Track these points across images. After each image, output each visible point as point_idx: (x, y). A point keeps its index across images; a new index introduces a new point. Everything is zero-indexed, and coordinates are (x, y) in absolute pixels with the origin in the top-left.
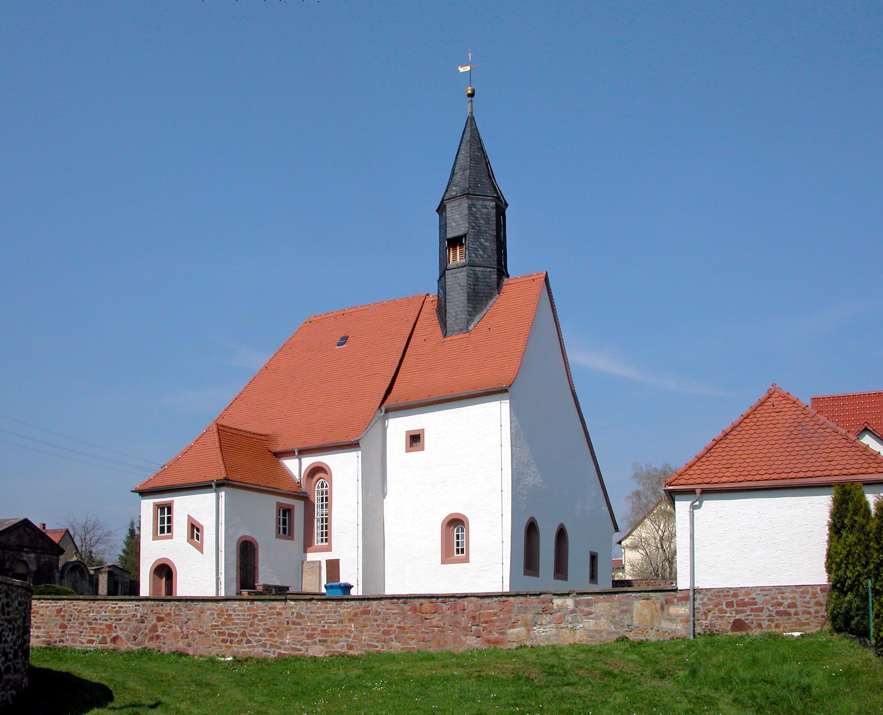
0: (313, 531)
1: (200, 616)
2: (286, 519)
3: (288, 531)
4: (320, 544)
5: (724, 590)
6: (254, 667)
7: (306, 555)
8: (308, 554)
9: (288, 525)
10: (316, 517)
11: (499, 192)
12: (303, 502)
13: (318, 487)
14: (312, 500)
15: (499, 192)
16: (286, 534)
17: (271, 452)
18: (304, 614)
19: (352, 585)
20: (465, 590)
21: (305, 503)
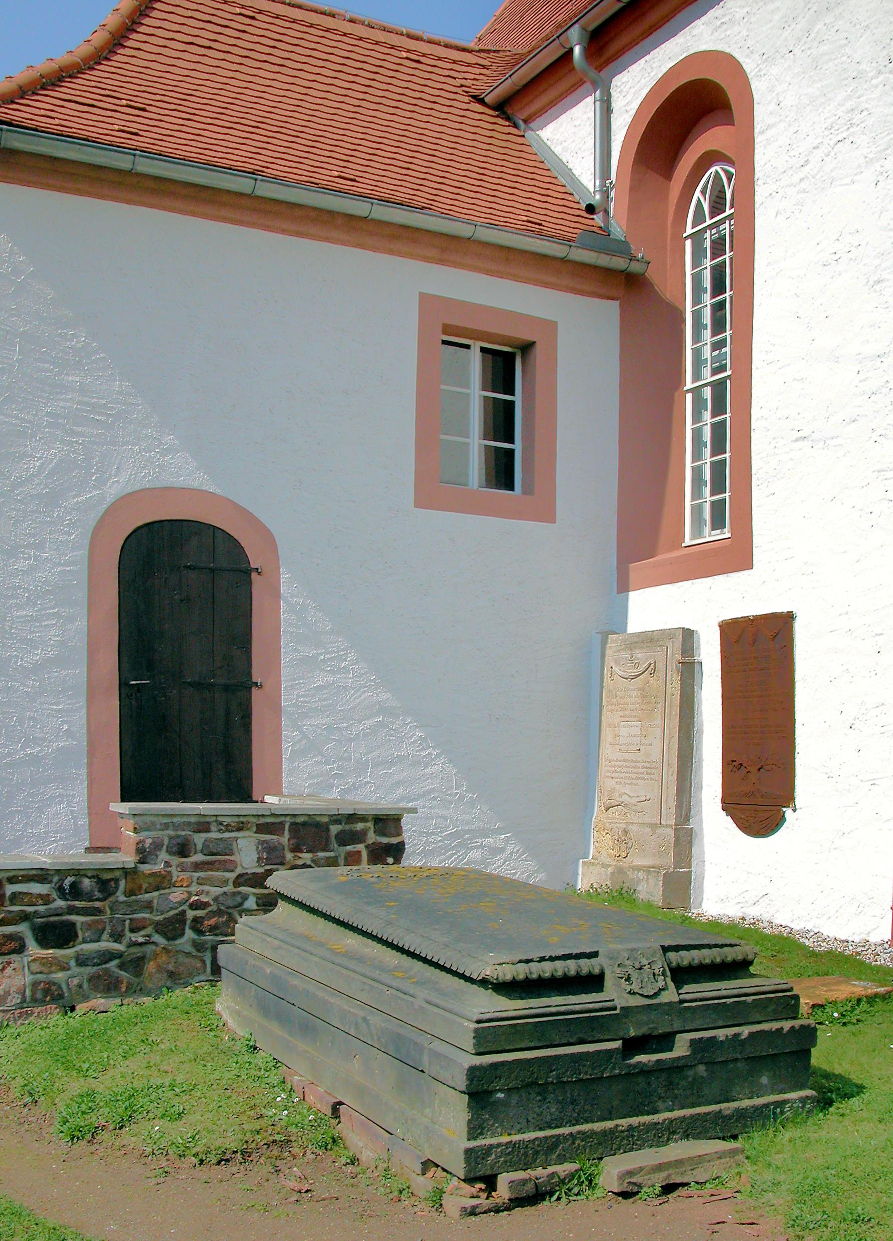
0: (682, 350)
1: (678, 1174)
2: (510, 453)
3: (524, 426)
4: (710, 535)
5: (282, 824)
6: (310, 1118)
7: (627, 599)
8: (636, 599)
9: (523, 439)
10: (689, 385)
11: (537, 1020)
12: (612, 309)
13: (699, 217)
14: (668, 293)
15: (537, 1020)
16: (510, 486)
17: (481, 101)
18: (686, 988)
19: (856, 1078)
20: (304, 873)
21: (621, 306)
